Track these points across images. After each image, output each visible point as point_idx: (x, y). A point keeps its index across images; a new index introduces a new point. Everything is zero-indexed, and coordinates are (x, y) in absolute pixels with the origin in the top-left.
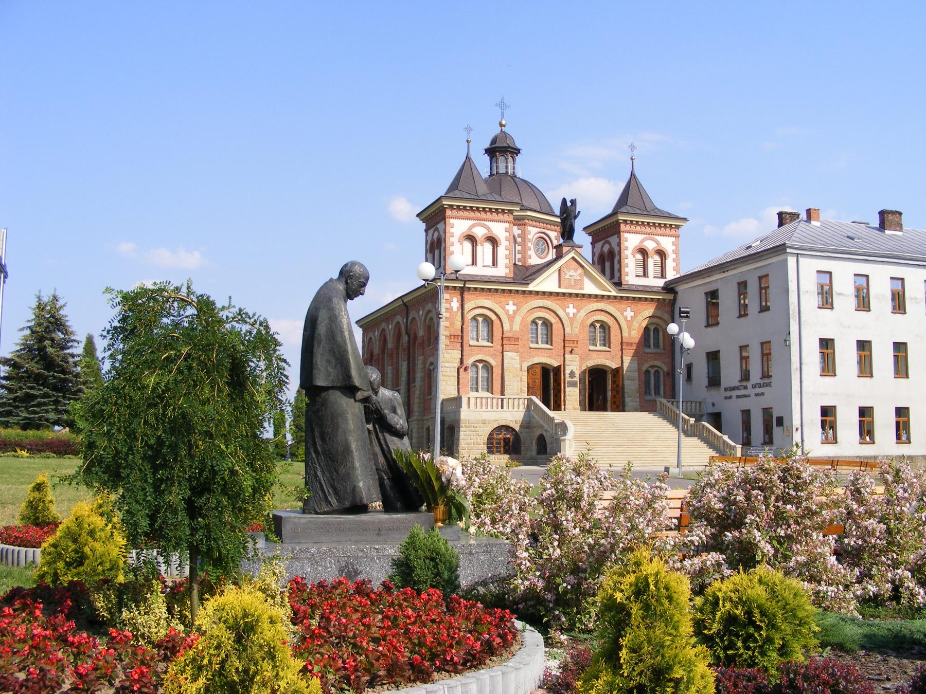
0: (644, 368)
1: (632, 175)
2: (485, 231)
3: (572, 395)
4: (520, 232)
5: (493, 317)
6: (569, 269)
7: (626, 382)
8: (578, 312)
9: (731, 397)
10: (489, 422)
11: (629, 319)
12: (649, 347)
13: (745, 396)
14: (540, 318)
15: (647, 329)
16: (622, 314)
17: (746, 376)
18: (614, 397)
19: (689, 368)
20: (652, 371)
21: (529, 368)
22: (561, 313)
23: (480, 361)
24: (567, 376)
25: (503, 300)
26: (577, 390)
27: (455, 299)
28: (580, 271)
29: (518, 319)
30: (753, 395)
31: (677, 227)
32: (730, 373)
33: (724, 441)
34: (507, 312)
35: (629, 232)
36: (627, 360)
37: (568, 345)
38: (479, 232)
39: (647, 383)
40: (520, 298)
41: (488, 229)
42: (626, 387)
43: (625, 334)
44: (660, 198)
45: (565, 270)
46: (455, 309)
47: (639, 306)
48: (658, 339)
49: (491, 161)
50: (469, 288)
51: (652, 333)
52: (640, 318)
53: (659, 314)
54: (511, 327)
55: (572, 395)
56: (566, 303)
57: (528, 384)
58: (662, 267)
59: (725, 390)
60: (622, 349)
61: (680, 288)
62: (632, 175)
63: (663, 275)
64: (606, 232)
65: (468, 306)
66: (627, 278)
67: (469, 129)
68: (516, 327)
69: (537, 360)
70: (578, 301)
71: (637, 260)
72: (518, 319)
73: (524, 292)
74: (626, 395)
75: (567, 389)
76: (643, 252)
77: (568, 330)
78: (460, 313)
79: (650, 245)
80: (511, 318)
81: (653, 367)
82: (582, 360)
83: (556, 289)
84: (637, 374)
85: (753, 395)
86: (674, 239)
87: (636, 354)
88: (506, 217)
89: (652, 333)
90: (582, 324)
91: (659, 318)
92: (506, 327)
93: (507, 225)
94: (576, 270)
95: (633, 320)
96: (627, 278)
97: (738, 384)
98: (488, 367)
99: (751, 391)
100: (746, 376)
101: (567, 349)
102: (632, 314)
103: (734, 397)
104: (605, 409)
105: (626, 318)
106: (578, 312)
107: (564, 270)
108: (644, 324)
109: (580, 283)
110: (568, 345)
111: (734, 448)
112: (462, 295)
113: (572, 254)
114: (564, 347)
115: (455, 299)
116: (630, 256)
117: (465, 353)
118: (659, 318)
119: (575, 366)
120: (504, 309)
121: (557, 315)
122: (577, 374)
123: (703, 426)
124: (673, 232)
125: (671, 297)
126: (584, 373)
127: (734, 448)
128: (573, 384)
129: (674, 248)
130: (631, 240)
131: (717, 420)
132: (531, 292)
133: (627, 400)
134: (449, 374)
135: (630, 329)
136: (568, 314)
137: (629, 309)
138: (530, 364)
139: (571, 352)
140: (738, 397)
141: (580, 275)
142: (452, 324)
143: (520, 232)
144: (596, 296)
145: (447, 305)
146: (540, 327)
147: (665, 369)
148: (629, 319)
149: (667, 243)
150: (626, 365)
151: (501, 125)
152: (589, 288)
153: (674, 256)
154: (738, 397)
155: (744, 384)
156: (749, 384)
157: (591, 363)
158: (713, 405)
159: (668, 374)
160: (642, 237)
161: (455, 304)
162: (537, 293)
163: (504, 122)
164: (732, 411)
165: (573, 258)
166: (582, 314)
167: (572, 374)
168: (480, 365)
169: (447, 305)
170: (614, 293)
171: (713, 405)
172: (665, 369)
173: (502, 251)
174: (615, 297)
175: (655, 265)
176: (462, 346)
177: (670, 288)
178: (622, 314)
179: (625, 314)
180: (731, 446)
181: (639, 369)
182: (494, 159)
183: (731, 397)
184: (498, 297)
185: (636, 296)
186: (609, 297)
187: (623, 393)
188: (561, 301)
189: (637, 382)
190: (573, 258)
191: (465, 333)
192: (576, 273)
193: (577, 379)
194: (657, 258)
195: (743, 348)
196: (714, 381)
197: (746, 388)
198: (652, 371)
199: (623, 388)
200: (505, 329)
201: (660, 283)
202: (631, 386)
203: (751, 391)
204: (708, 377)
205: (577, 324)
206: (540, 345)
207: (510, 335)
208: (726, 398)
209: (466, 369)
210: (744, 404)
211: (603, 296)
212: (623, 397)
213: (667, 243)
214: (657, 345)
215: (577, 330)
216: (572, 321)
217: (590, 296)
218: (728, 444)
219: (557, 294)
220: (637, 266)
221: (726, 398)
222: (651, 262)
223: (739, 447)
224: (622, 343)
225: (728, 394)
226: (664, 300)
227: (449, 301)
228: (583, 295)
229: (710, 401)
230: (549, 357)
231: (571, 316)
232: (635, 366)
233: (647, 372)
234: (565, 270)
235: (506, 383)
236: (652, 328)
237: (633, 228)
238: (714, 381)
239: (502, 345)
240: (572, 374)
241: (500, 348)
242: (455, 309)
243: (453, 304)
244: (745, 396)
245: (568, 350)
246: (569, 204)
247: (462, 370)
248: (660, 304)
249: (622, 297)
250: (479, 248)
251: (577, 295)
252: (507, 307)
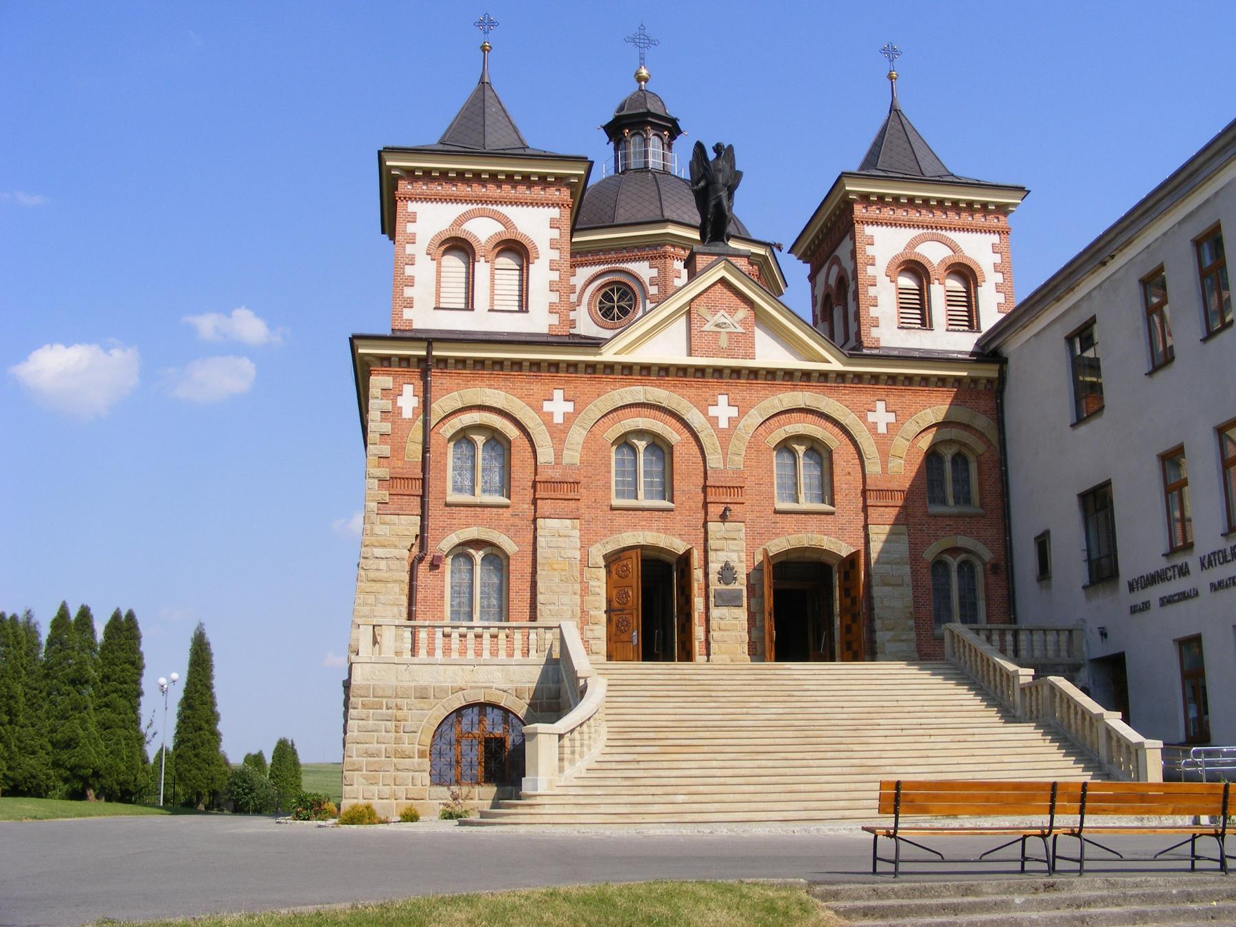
0: (929, 554)
1: (894, 110)
2: (499, 228)
3: (726, 627)
4: (654, 272)
5: (512, 431)
6: (714, 309)
7: (877, 591)
8: (742, 413)
9: (1146, 606)
10: (440, 693)
11: (882, 429)
12: (944, 502)
13: (1183, 596)
14: (640, 433)
15: (932, 456)
16: (863, 418)
17: (1180, 545)
18: (847, 629)
19: (1043, 542)
20: (953, 563)
21: (613, 560)
22: (695, 417)
23: (478, 544)
24: (713, 577)
25: (537, 388)
26: (742, 614)
27: (408, 389)
28: (743, 312)
29: (577, 435)
30: (1205, 591)
31: (1002, 209)
32: (1140, 540)
33: (1109, 731)
34: (547, 418)
35: (876, 223)
36: (879, 535)
37: (718, 499)
38: (483, 230)
39: (942, 593)
40: (584, 384)
41: (505, 221)
42: (877, 603)
43: (873, 468)
44: (953, 145)
45: (703, 311)
46: (407, 413)
47: (909, 397)
48: (967, 481)
49: (616, 149)
50: (443, 361)
51: (948, 466)
52: (912, 427)
53: (963, 415)
54: (558, 455)
55: (726, 627)
56: (707, 393)
57: (609, 601)
58: (969, 306)
59: (1131, 587)
60: (865, 508)
61: (1013, 347)
62: (894, 110)
63: (972, 323)
64: (829, 239)
65: (440, 406)
66: (875, 332)
67: (486, 24)
68: (572, 456)
69: (630, 538)
70: (741, 389)
71: (902, 291)
72: (577, 435)
73: (592, 367)
74: (878, 624)
75: (715, 613)
76: (915, 268)
77: (714, 460)
78: (419, 423)
79: (934, 254)
80: (559, 434)
81: (954, 551)
82: (754, 536)
83: (678, 357)
84: (907, 569)
85: (1205, 591)
86: (995, 238)
87: (904, 519)
88: (553, 193)
89: (948, 466)
90: (754, 445)
91: (966, 427)
92: (546, 454)
93: (555, 212)
94: (732, 311)
95: (893, 435)
96: (875, 332)
97: (1163, 564)
98: (497, 558)
99: (1200, 579)
100: (1180, 545)
101: (711, 508)
102: (891, 418)
103: (1155, 603)
104: (832, 659)
105: (873, 428)
106: (742, 413)
107: (701, 309)
108: (925, 442)
109: (744, 343)
110: (718, 499)
111: (1136, 752)
112: (424, 376)
113: (719, 272)
114: (705, 505)
115: (408, 389)
116: (883, 280)
117: (431, 523)
118: (966, 427)
119: (734, 551)
120: (538, 409)
121: (686, 425)
122: (742, 572)
123: (1053, 687)
124: (992, 221)
125: (989, 371)
126: (759, 569)
127: (1136, 752)
128: (729, 600)
129: (997, 258)
130: (881, 244)
131: (1113, 680)
132: (609, 367)
133: (881, 636)
134: (383, 575)
135: (885, 456)
136: (714, 421)
137: (881, 406)
138: (610, 548)
139: (723, 518)
140: (1166, 601)
141: (743, 322)
142: (398, 449)
143: (654, 272)
144: (789, 374)
145: (387, 404)
146: (641, 457)
147: (988, 555)
148: (882, 429)
149: (979, 248)
150: (876, 547)
151: (640, 79)
152: (769, 353)
153: (999, 278)
154: (1166, 601)
155: (1179, 560)
156: (1192, 561)
157: (778, 545)
158: (1104, 634)
159: (995, 568)
160: (910, 234)
161: (408, 401)
162: (628, 369)
163: (644, 72)
164: (1151, 647)
165: (723, 281)
166: (755, 417)
167: (727, 573)
168: (478, 555)
169: (387, 404)
170: (836, 365)
171: (1104, 634)
172: (988, 555)
173: (540, 274)
174: (841, 376)
175: (950, 303)
176: (423, 506)
177: (990, 352)
178: (863, 418)
179: (871, 417)
180: (1129, 745)
181: (915, 558)
182: (622, 145)
183: (1146, 606)
184: (523, 382)
185: (904, 376)
186: (824, 375)
187: (871, 619)
188: (696, 389)
189: (908, 591)
190: (723, 281)
191: (432, 474)
192: (734, 318)
193: (740, 585)
194: (955, 284)
195: (1172, 458)
196: (1103, 570)
197: (1184, 571)
198: (953, 563)
199: (871, 608)
200: (540, 459)
201: (966, 342)
202: (892, 602)
203: (1200, 579)
204: (1089, 560)
205: (739, 446)
206: (643, 502)
207: (556, 475)
208: (1134, 610)
209: (434, 566)
210: (1183, 619)
211: (807, 375)
212: (872, 631)
213: (979, 248)
214: (963, 497)
215: (738, 462)
216: (725, 437)
217: (771, 374)
218: (1120, 739)
219: (682, 370)
220: (903, 305)
221: (1134, 610)
222: (937, 293)
223: (1153, 752)
224: (864, 492)
225: (1140, 597)
226: (974, 380)
227: (392, 394)
228: (754, 373)
229: (1093, 627)
230: (666, 530)
231: (723, 424)
232: (903, 547)
233: (939, 566)
234: (703, 311)
235: (540, 598)
236: (948, 453)
237: (887, 213)
238: (1103, 570)
239: (534, 502)
240: (727, 573)
241: (527, 507)
242: (407, 413)
243: (401, 402)
244: (1183, 596)
245: (716, 510)
246: (711, 156)
247: (423, 568)
248: (964, 390)
249: (859, 377)
250: (482, 269)
251: (736, 372)
252: (547, 407)
